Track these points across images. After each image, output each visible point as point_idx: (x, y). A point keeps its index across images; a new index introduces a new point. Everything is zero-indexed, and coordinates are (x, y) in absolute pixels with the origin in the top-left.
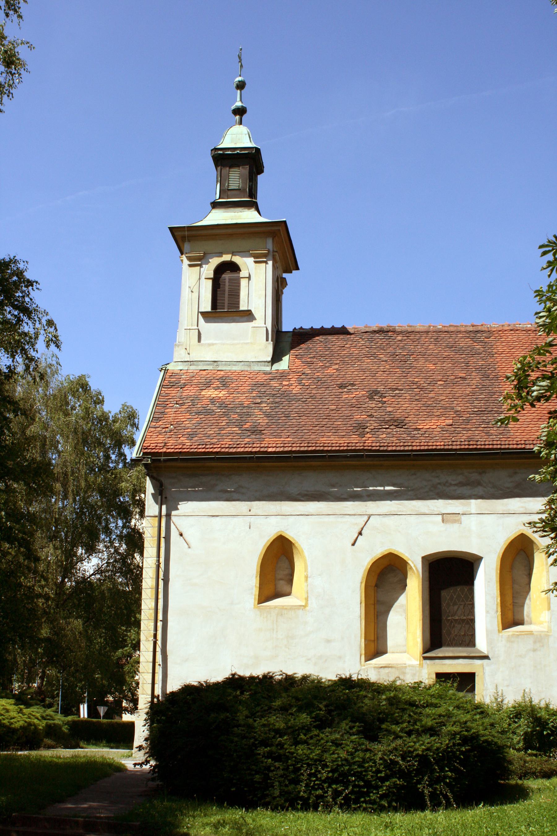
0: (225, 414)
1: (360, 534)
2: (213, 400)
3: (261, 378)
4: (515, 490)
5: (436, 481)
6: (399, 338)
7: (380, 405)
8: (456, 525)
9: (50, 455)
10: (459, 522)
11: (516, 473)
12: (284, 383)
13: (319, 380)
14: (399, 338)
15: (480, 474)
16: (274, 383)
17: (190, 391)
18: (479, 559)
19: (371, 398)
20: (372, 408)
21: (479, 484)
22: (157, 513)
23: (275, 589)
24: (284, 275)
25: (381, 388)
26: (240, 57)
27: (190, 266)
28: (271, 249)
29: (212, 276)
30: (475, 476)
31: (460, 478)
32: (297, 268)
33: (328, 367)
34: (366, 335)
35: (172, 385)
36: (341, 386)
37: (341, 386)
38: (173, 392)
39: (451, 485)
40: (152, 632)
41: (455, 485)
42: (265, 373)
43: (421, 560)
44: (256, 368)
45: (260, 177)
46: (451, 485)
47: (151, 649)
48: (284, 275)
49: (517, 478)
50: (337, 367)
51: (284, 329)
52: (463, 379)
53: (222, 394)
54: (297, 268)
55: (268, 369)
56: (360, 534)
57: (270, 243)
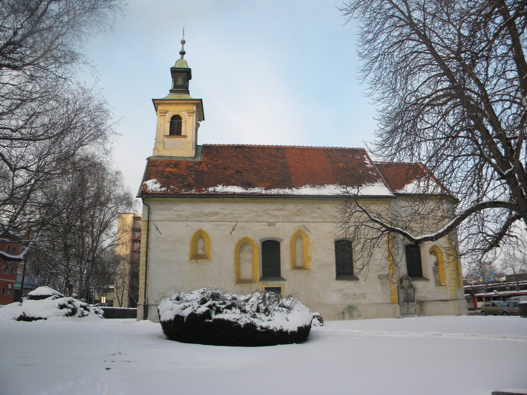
0: (176, 179)
1: (234, 229)
2: (171, 172)
3: (190, 164)
4: (298, 213)
5: (265, 208)
6: (247, 150)
7: (241, 177)
8: (273, 227)
9: (456, 48)
10: (275, 225)
11: (298, 206)
12: (201, 166)
13: (215, 165)
14: (247, 150)
15: (283, 206)
16: (196, 166)
17: (160, 169)
18: (282, 240)
19: (237, 174)
20: (238, 178)
21: (282, 210)
22: (147, 219)
23: (430, 301)
24: (199, 122)
25: (241, 170)
26: (183, 31)
27: (160, 116)
28: (195, 111)
29: (170, 121)
30: (281, 207)
31: (275, 208)
32: (204, 120)
33: (219, 160)
34: (233, 148)
35: (153, 166)
36: (225, 168)
37: (225, 168)
38: (153, 169)
39: (271, 210)
40: (145, 271)
41: (273, 210)
42: (192, 162)
43: (333, 247)
44: (188, 160)
45: (190, 81)
46: (271, 210)
47: (144, 278)
48: (199, 122)
49: (298, 208)
50: (222, 160)
51: (198, 144)
52: (274, 167)
53: (174, 170)
54: (204, 120)
55: (193, 160)
56: (234, 229)
57: (194, 108)
